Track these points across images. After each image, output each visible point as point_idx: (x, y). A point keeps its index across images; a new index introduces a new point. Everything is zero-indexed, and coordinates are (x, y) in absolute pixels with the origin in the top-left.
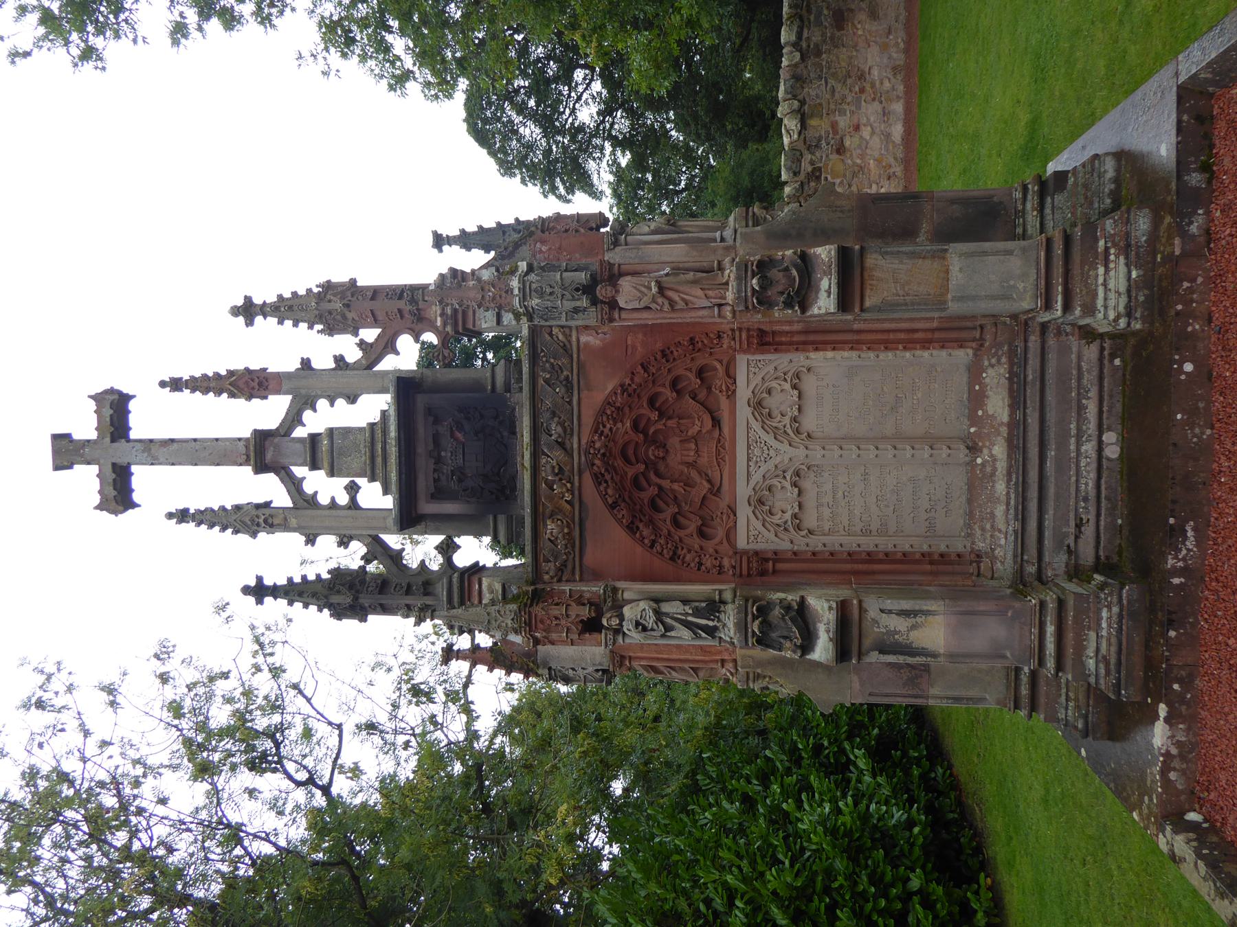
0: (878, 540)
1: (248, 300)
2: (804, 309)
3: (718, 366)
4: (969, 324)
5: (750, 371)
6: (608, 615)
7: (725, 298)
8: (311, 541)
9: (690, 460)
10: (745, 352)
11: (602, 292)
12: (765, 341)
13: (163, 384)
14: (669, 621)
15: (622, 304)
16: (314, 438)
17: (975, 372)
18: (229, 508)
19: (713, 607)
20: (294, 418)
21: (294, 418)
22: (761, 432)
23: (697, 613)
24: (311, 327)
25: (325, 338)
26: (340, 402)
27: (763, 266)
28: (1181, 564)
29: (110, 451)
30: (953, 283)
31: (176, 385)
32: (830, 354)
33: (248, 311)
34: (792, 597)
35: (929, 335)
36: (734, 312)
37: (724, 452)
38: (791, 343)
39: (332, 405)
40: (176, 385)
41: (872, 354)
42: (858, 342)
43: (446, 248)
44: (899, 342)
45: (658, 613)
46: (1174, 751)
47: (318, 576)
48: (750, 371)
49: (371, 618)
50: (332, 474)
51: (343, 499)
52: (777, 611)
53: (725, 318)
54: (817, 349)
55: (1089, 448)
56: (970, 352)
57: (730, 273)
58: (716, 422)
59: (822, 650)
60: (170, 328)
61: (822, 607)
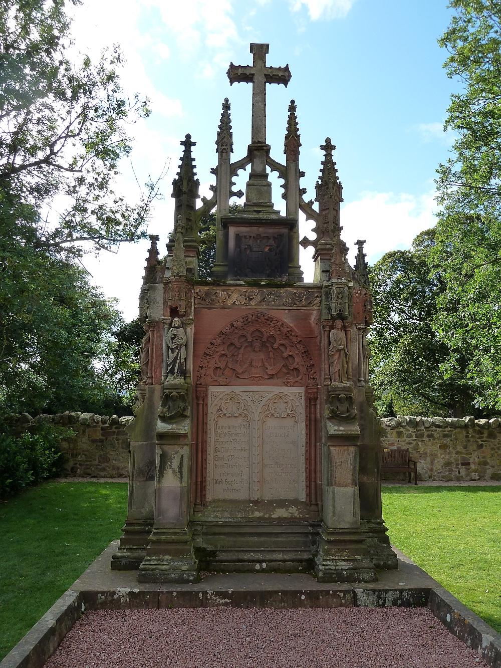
0: (212, 456)
1: (334, 147)
2: (330, 419)
3: (300, 378)
4: (318, 499)
5: (295, 394)
6: (180, 321)
7: (334, 381)
8: (213, 171)
9: (254, 364)
10: (306, 392)
11: (339, 323)
12: (311, 401)
13: (293, 102)
14: (177, 350)
15: (332, 332)
16: (266, 176)
17: (295, 502)
18: (231, 131)
19: (183, 373)
20: (275, 166)
21: (275, 166)
22: (266, 399)
23: (181, 365)
24: (320, 178)
25: (314, 184)
26: (283, 190)
27: (350, 399)
28: (209, 597)
29: (258, 72)
30: (341, 489)
31: (292, 108)
32: (304, 432)
33: (328, 147)
34: (188, 413)
35: (313, 480)
36: (328, 385)
37: (256, 380)
38: (310, 413)
39: (281, 186)
40: (292, 108)
41: (304, 452)
42: (310, 446)
43: (357, 246)
44: (310, 466)
45: (181, 345)
46: (115, 597)
47: (196, 174)
48: (295, 394)
49: (174, 200)
50: (248, 185)
51: (235, 189)
52: (182, 405)
53: (324, 381)
54: (307, 426)
55: (259, 556)
56: (304, 500)
57: (347, 384)
58: (272, 377)
59: (161, 426)
60: (323, 109)
61: (185, 427)
